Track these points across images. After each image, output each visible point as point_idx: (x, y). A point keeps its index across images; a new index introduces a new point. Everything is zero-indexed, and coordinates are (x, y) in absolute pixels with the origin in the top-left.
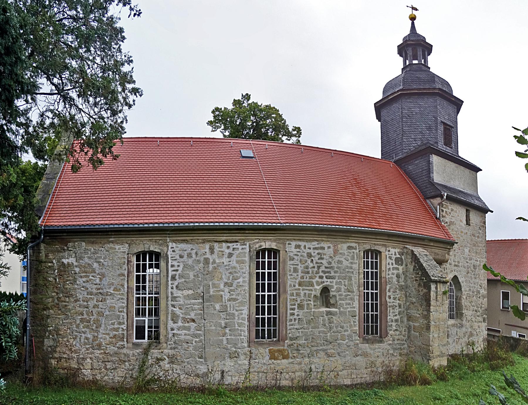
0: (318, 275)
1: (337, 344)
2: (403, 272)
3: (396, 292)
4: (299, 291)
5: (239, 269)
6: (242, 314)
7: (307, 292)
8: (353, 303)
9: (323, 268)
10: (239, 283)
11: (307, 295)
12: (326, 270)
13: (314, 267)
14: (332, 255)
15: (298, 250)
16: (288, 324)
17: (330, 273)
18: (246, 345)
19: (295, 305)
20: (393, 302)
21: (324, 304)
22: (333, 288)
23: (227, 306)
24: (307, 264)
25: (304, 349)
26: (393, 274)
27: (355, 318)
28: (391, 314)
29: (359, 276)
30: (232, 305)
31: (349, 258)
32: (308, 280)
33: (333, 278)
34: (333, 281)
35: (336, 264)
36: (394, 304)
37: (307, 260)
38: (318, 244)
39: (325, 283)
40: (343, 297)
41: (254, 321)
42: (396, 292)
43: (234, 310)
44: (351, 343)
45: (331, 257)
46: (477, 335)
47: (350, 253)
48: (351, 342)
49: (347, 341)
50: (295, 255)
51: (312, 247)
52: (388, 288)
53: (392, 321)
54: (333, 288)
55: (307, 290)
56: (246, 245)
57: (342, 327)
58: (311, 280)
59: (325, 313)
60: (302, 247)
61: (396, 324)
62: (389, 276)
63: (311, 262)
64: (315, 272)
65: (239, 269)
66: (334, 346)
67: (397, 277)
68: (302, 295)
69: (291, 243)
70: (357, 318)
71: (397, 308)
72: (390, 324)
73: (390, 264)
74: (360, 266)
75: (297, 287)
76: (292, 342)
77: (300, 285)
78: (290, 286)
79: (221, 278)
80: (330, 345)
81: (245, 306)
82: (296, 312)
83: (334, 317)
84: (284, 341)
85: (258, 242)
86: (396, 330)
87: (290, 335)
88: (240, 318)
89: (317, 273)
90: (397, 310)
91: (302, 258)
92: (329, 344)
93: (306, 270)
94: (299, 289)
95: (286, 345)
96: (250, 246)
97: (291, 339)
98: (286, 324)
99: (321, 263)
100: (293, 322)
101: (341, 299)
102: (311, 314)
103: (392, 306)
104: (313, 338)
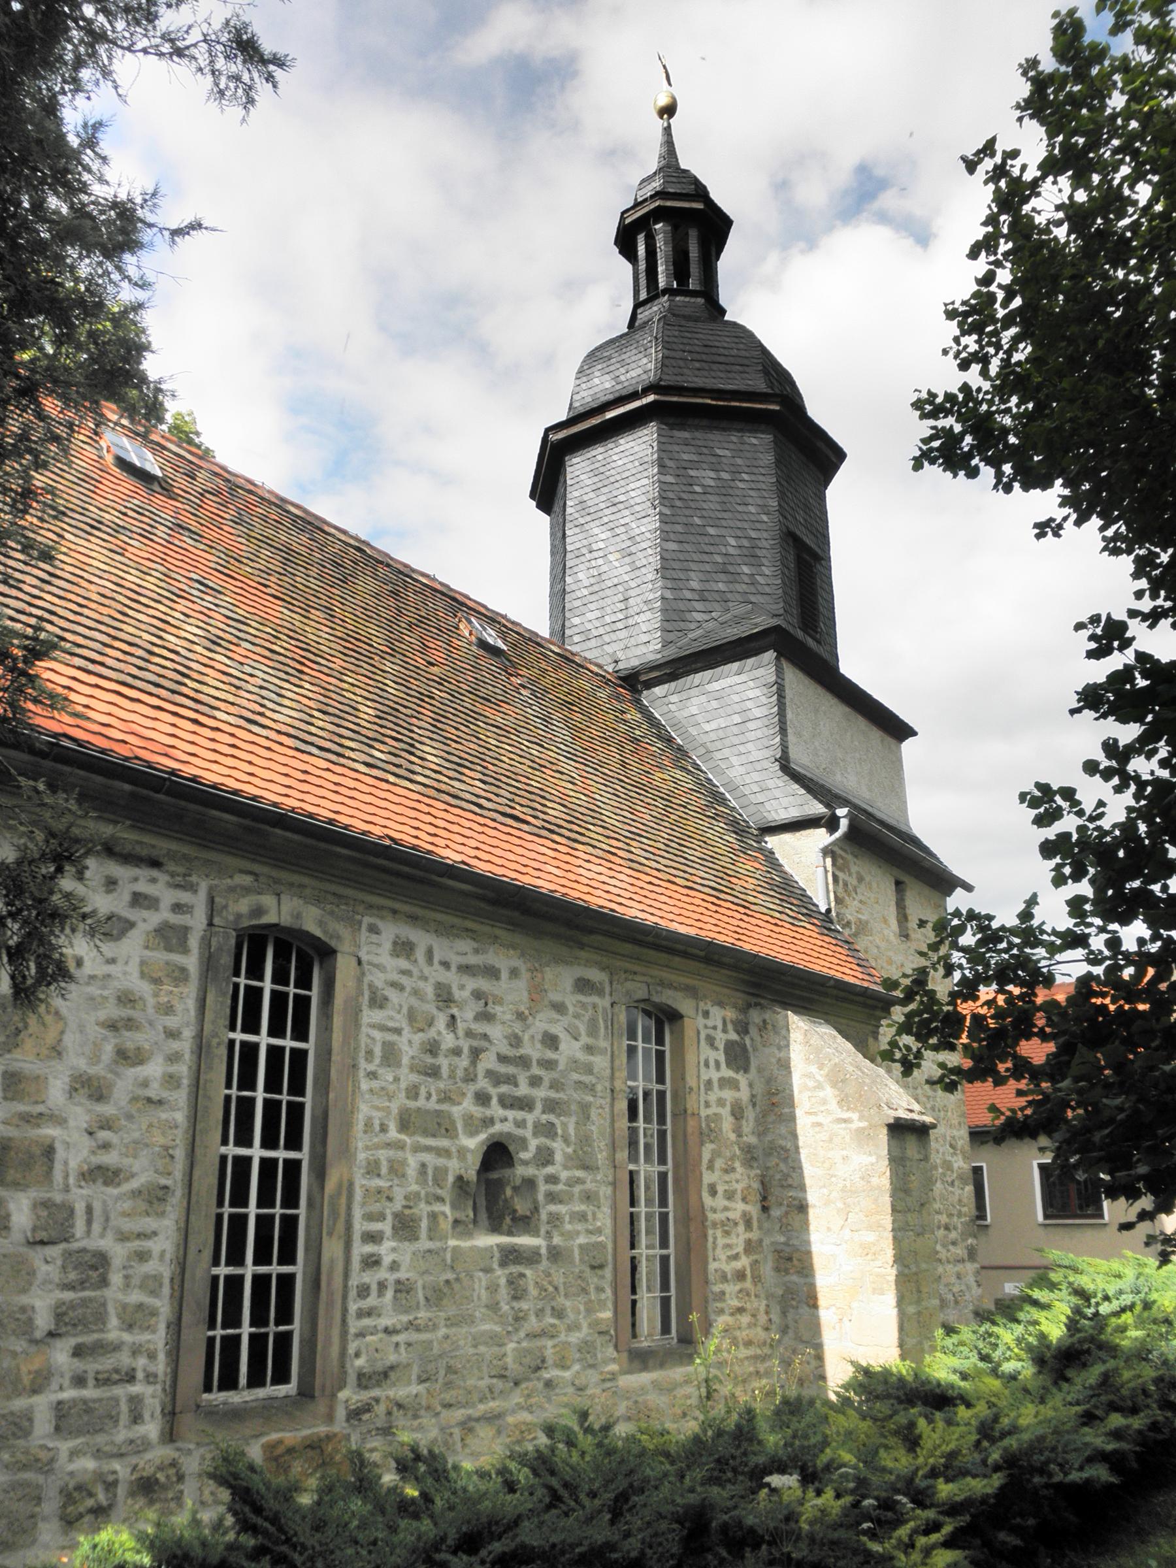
0: (471, 1089)
1: (540, 1385)
2: (753, 1096)
3: (733, 1170)
4: (400, 1153)
5: (150, 1011)
6: (143, 1256)
7: (428, 1158)
8: (594, 1214)
9: (488, 1061)
10: (145, 1084)
11: (430, 1172)
12: (503, 1069)
13: (457, 1052)
14: (522, 1008)
15: (403, 964)
16: (353, 1307)
17: (516, 1085)
18: (151, 1429)
19: (381, 1217)
20: (726, 1209)
21: (483, 1215)
22: (525, 1149)
23: (72, 1212)
24: (432, 1033)
25: (416, 1423)
26: (721, 1102)
27: (600, 1272)
28: (719, 1251)
29: (612, 1106)
30: (97, 1207)
31: (582, 1029)
32: (433, 1105)
33: (525, 1104)
34: (524, 1121)
35: (539, 1046)
36: (731, 1215)
37: (433, 1018)
38: (477, 951)
39: (498, 1128)
40: (560, 1187)
41: (198, 1291)
42: (733, 1170)
43: (110, 1235)
44: (593, 1377)
45: (520, 1016)
46: (956, 1302)
47: (584, 1006)
48: (590, 1371)
49: (577, 1367)
50: (394, 985)
51: (455, 960)
52: (706, 1156)
53: (724, 1278)
54: (525, 1149)
55: (428, 1149)
56: (192, 888)
57: (559, 1314)
58: (444, 1107)
59: (497, 1255)
60: (420, 954)
61: (738, 1287)
62: (710, 1111)
63: (448, 1026)
64: (460, 1073)
65: (150, 1011)
66: (529, 1396)
67: (733, 1114)
68: (412, 1171)
69: (380, 924)
70: (608, 1272)
71: (741, 1228)
72: (717, 1288)
73: (712, 1063)
74: (617, 1063)
75: (393, 1134)
76: (365, 1396)
77: (405, 1125)
78: (368, 1124)
79: (57, 1051)
80: (518, 1391)
81: (162, 1214)
82: (386, 1250)
83: (528, 1272)
84: (333, 1396)
85: (247, 890)
86: (741, 1310)
87: (359, 1362)
88: (135, 1281)
89: (470, 1078)
90: (739, 1239)
91: (413, 1001)
92: (511, 1390)
93: (429, 1060)
94: (400, 1146)
95: (341, 1413)
96: (211, 901)
97: (364, 1380)
98: (345, 1311)
99: (485, 1036)
100: (371, 1301)
101: (552, 1197)
102: (444, 1260)
103: (723, 1224)
104: (450, 1370)
